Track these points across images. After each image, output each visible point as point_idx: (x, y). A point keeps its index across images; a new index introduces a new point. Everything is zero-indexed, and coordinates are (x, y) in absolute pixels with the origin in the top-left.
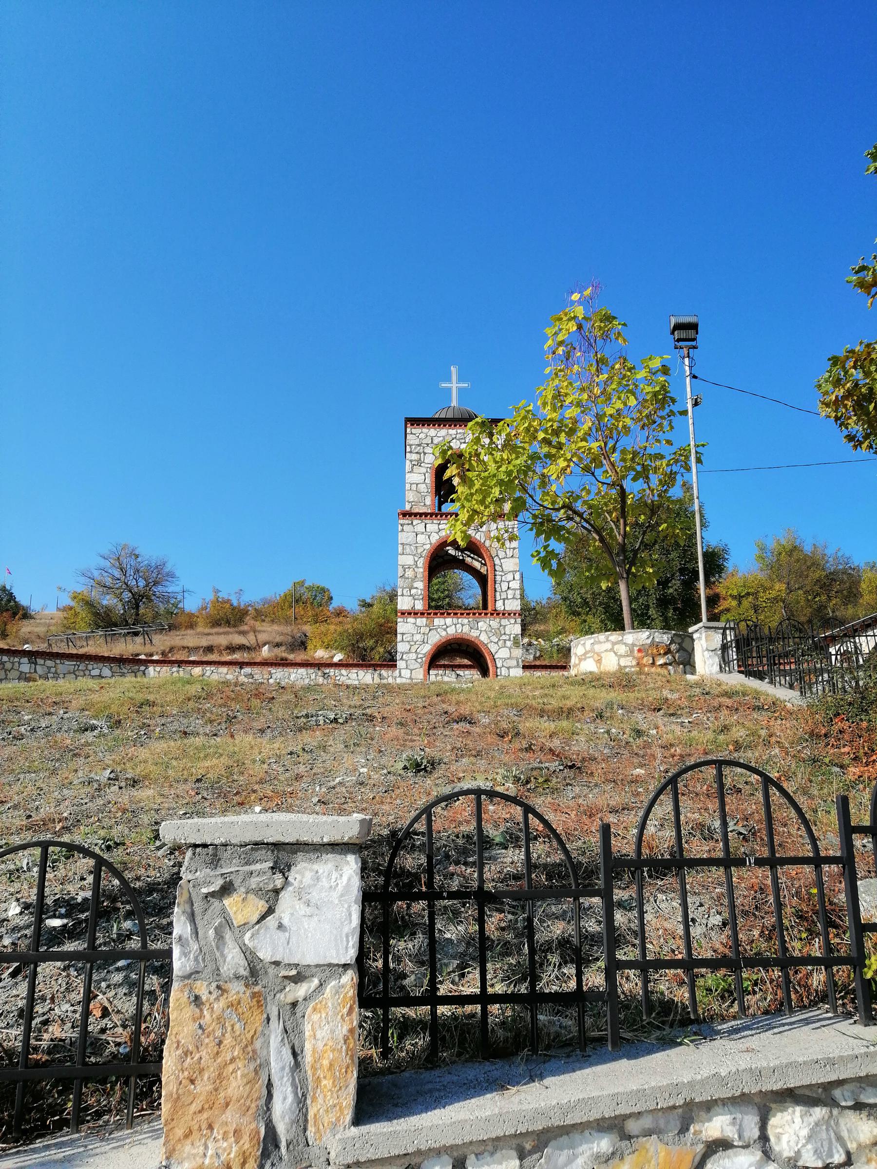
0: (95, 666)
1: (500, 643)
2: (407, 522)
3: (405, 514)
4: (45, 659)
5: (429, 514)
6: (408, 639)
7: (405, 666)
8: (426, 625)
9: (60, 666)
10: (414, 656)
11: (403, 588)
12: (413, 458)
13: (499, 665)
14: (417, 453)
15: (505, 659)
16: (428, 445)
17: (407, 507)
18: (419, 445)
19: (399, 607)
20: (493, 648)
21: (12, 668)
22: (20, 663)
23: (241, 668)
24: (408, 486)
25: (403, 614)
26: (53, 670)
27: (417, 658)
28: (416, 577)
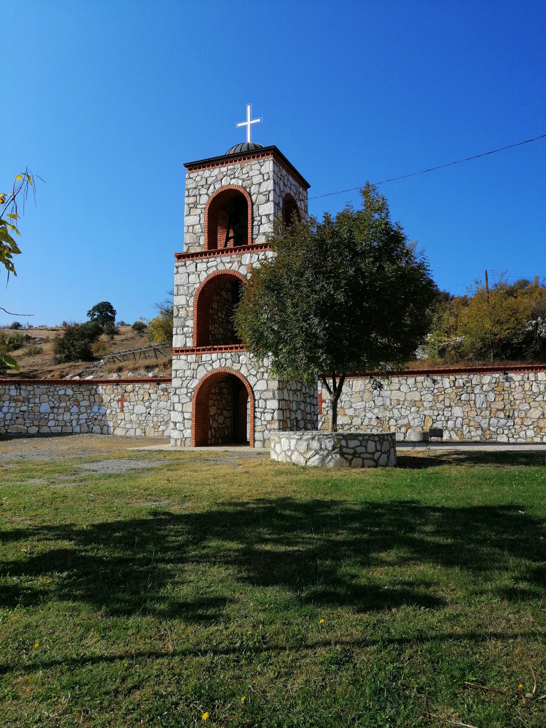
0: (61, 388)
1: (259, 375)
2: (181, 264)
3: (180, 257)
4: (26, 385)
5: (199, 253)
6: (180, 375)
7: (177, 401)
8: (196, 362)
9: (37, 390)
10: (184, 391)
11: (177, 327)
12: (190, 202)
13: (257, 397)
14: (194, 196)
15: (263, 391)
16: (202, 186)
17: (185, 249)
18: (195, 188)
19: (174, 346)
20: (252, 380)
21: (5, 393)
22: (9, 390)
23: (158, 384)
24: (185, 229)
25: (177, 351)
26: (32, 393)
27: (188, 393)
28: (188, 316)
